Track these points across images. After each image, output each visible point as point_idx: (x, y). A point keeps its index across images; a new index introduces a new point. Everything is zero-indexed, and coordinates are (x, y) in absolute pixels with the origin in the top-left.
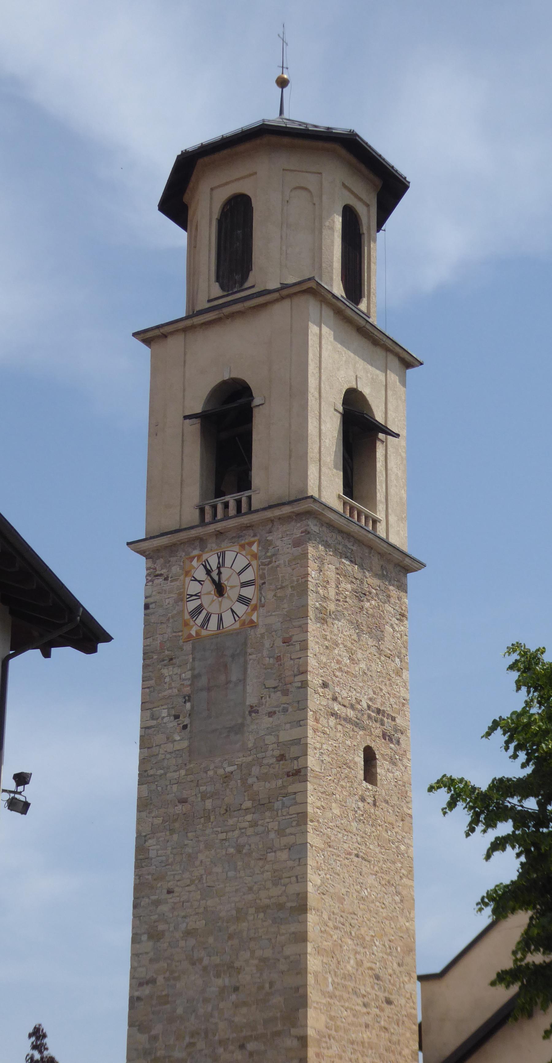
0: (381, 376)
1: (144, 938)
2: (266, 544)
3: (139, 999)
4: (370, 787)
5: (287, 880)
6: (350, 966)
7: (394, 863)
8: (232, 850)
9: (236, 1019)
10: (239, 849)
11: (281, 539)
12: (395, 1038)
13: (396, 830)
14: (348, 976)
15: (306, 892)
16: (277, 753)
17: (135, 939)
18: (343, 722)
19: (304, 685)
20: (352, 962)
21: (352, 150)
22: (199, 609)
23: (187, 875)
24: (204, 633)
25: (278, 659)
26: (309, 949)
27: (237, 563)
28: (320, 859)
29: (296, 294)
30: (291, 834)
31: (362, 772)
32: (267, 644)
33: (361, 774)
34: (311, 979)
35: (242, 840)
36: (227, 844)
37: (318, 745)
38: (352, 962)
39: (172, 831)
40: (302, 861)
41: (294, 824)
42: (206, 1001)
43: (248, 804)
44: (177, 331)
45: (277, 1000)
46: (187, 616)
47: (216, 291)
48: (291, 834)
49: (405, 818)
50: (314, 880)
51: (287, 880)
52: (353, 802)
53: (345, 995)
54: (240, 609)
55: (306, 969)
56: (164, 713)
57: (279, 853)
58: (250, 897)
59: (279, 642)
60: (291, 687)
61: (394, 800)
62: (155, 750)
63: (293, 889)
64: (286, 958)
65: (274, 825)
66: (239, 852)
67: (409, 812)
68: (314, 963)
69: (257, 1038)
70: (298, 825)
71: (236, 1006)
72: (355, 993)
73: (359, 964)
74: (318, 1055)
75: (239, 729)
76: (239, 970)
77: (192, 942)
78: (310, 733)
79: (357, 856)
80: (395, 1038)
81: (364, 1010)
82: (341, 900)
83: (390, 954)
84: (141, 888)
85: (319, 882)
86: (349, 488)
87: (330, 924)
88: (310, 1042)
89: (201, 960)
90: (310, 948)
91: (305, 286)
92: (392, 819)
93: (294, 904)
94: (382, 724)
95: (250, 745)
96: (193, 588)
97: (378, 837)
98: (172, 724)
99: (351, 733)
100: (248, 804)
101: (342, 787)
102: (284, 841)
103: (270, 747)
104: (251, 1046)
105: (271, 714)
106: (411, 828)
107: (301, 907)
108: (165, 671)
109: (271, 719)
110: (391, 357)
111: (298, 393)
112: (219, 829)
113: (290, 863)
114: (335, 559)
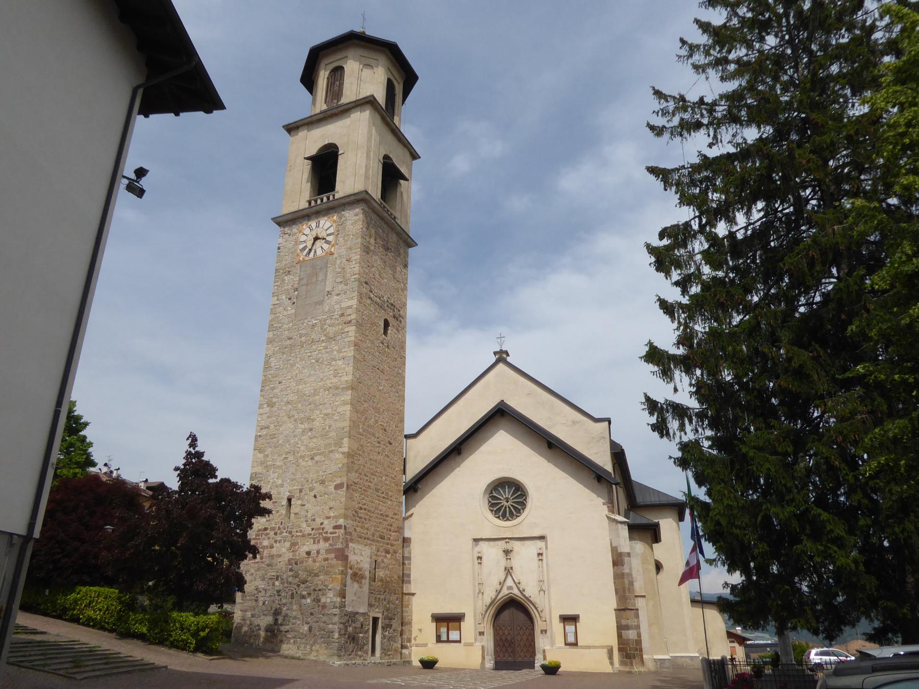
3: (260, 436)
6: (372, 422)
16: (340, 313)
24: (307, 258)
25: (343, 269)
32: (338, 262)
35: (320, 355)
39: (283, 353)
43: (324, 338)
45: (332, 434)
46: (299, 251)
52: (377, 343)
59: (344, 260)
73: (377, 422)
75: (321, 303)
76: (313, 420)
77: (290, 406)
86: (383, 196)
89: (293, 416)
98: (288, 302)
100: (324, 338)
102: (341, 355)
105: (338, 295)
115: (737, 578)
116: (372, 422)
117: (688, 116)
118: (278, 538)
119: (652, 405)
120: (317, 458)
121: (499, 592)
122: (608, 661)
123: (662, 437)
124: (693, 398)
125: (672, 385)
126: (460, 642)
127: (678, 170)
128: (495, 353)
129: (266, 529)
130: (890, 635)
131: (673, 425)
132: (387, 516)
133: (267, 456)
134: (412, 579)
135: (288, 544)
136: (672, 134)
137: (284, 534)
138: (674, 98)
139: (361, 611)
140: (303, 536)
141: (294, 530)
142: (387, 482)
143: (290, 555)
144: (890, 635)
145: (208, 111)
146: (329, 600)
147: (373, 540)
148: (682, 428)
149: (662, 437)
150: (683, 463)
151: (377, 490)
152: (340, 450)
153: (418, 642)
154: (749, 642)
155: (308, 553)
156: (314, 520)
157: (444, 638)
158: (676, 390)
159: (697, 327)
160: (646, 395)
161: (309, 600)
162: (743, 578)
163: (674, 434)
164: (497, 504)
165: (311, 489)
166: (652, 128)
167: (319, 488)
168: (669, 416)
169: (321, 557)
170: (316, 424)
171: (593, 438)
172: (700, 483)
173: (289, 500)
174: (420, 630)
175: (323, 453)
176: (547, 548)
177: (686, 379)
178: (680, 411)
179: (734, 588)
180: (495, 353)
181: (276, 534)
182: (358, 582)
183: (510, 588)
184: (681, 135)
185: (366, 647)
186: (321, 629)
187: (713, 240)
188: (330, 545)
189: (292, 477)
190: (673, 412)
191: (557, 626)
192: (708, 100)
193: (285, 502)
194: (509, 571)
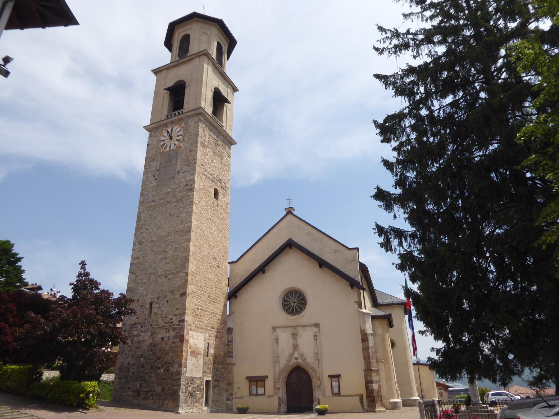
0: (227, 89)
1: (137, 244)
2: (186, 124)
3: (133, 264)
11: (191, 122)
12: (220, 279)
17: (134, 245)
19: (195, 163)
21: (220, 24)
22: (164, 144)
23: (153, 224)
25: (188, 156)
27: (177, 130)
28: (197, 217)
29: (201, 55)
33: (213, 196)
34: (191, 254)
39: (149, 210)
40: (191, 216)
42: (155, 263)
43: (175, 200)
44: (165, 69)
45: (179, 261)
47: (178, 58)
50: (194, 223)
53: (203, 262)
54: (177, 143)
56: (150, 175)
58: (173, 229)
60: (191, 164)
62: (146, 187)
65: (182, 206)
66: (170, 215)
68: (192, 249)
71: (165, 264)
73: (209, 253)
74: (192, 279)
75: (173, 178)
76: (167, 252)
77: (152, 244)
78: (196, 177)
82: (204, 231)
84: (138, 229)
90: (191, 244)
91: (204, 53)
96: (163, 138)
97: (218, 216)
98: (152, 178)
100: (175, 200)
102: (185, 210)
104: (169, 277)
105: (184, 173)
107: (189, 230)
108: (152, 163)
110: (229, 85)
111: (199, 82)
114: (209, 131)
115: (440, 344)
117: (402, 42)
118: (143, 329)
119: (380, 230)
120: (169, 277)
121: (289, 361)
122: (359, 405)
123: (387, 251)
124: (407, 222)
125: (392, 214)
126: (264, 394)
127: (394, 75)
129: (136, 324)
130: (544, 381)
131: (395, 242)
132: (216, 314)
133: (137, 276)
135: (149, 334)
136: (389, 52)
137: (147, 327)
138: (391, 31)
139: (198, 376)
140: (160, 327)
141: (154, 324)
142: (217, 292)
143: (151, 341)
144: (544, 381)
145: (66, 25)
146: (175, 370)
148: (400, 244)
149: (387, 251)
150: (402, 267)
151: (209, 297)
153: (238, 395)
154: (450, 389)
155: (162, 339)
156: (166, 317)
157: (254, 392)
158: (395, 217)
159: (408, 174)
160: (376, 223)
161: (162, 370)
162: (445, 344)
163: (395, 249)
164: (288, 305)
165: (165, 297)
166: (377, 49)
167: (170, 296)
168: (392, 237)
169: (170, 341)
170: (169, 255)
171: (348, 261)
172: (414, 281)
173: (151, 304)
174: (239, 388)
175: (173, 273)
176: (319, 332)
177: (402, 210)
178: (399, 234)
179: (438, 351)
180: (285, 209)
181: (142, 327)
182: (195, 357)
183: (296, 358)
184: (395, 54)
185: (201, 400)
187: (420, 119)
188: (177, 333)
190: (394, 234)
191: (327, 382)
192: (412, 31)
193: (148, 306)
194: (295, 347)
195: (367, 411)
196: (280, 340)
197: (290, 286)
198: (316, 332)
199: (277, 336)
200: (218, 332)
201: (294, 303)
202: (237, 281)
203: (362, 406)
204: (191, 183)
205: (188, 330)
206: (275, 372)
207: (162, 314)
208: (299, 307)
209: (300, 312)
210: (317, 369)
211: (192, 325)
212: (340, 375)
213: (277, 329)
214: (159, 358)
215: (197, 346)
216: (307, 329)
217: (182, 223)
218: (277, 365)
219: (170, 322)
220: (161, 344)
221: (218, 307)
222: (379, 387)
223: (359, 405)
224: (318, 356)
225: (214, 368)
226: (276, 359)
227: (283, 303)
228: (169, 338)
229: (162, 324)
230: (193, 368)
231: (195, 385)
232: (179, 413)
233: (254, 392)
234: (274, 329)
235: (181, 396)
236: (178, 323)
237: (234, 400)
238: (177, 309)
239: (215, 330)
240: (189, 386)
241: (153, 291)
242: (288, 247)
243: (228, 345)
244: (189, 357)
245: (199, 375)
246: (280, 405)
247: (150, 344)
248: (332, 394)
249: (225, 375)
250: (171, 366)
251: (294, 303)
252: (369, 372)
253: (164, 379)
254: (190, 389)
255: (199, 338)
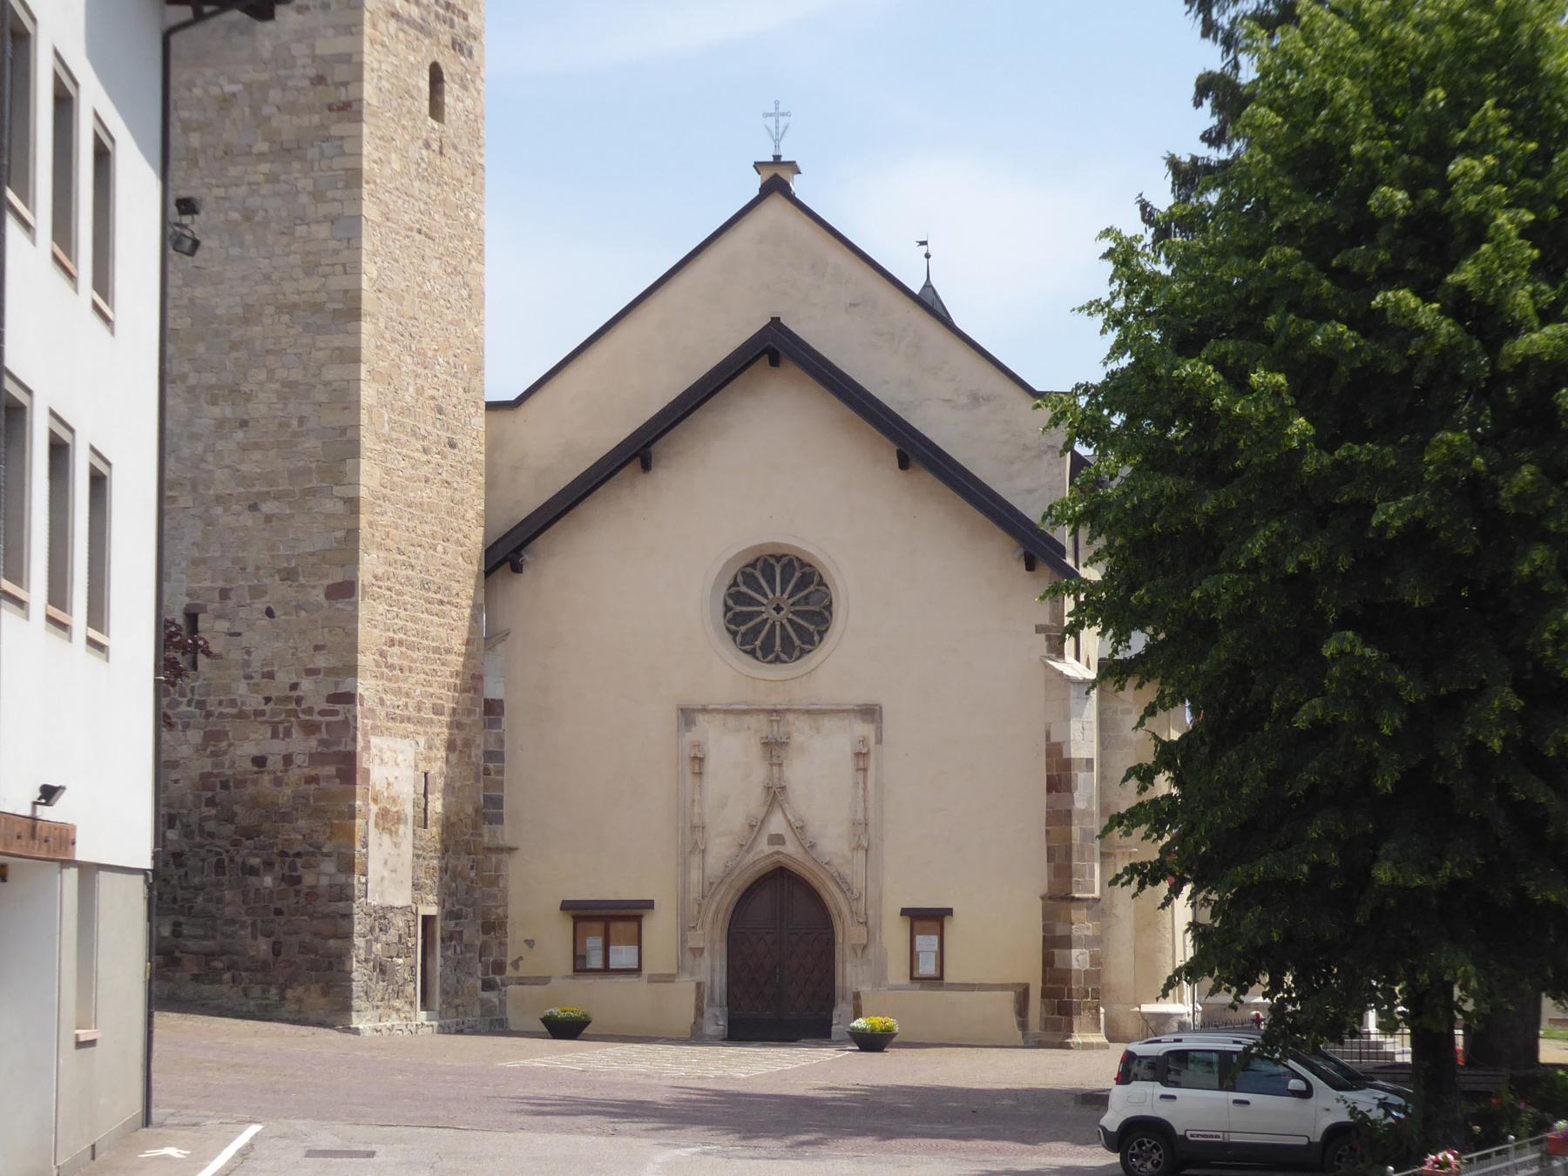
4: (436, 125)
5: (328, 270)
6: (408, 396)
7: (462, 240)
8: (235, 215)
9: (244, 468)
10: (248, 216)
12: (458, 496)
13: (466, 189)
14: (407, 411)
15: (359, 290)
16: (311, 72)
18: (405, 27)
20: (411, 389)
26: (363, 374)
28: (376, 240)
30: (335, 200)
31: (427, 103)
34: (364, 418)
35: (254, 202)
36: (227, 205)
37: (376, 65)
38: (411, 389)
41: (340, 185)
42: (194, 437)
43: (263, 147)
45: (311, 444)
48: (335, 200)
49: (475, 170)
51: (328, 270)
52: (416, 151)
53: (403, 438)
55: (359, 402)
57: (314, 228)
58: (266, 289)
61: (463, 147)
63: (339, 282)
64: (327, 384)
65: (306, 184)
67: (480, 161)
68: (368, 393)
69: (277, 497)
70: (347, 187)
71: (244, 448)
72: (414, 434)
73: (420, 391)
74: (371, 524)
76: (248, 397)
79: (419, 232)
80: (458, 496)
81: (425, 458)
83: (454, 376)
85: (375, 275)
87: (387, 336)
88: (363, 509)
92: (460, 173)
93: (339, 306)
94: (452, 26)
95: (266, 54)
99: (415, 43)
100: (263, 147)
101: (404, 127)
102: (323, 209)
103: (300, 62)
104: (268, 507)
106: (482, 187)
107: (352, 311)
109: (301, 17)
112: (214, 181)
113: (333, 244)
116: (408, 396)
121: (745, 847)
126: (637, 971)
128: (758, 166)
134: (505, 810)
135: (195, 736)
139: (399, 903)
140: (242, 715)
141: (212, 700)
142: (448, 558)
143: (207, 765)
146: (324, 881)
147: (420, 722)
151: (424, 585)
152: (337, 490)
153: (525, 970)
155: (260, 761)
156: (270, 676)
157: (595, 961)
161: (268, 881)
165: (257, 592)
167: (278, 591)
170: (257, 409)
171: (1025, 448)
174: (530, 943)
176: (879, 741)
180: (758, 166)
182: (391, 832)
183: (777, 839)
185: (409, 989)
186: (305, 949)
188: (322, 742)
189: (196, 553)
191: (894, 934)
194: (775, 795)
195: (1040, 1044)
196: (711, 765)
197: (765, 540)
198: (864, 741)
199: (698, 745)
200: (455, 725)
201: (778, 609)
202: (529, 498)
203: (1023, 1025)
204: (341, 72)
205: (365, 735)
206: (685, 889)
207: (247, 664)
208: (799, 629)
209: (803, 652)
210: (858, 883)
211: (379, 709)
212: (949, 912)
213: (700, 718)
214: (250, 833)
215: (394, 792)
216: (828, 724)
217: (310, 269)
218: (696, 860)
219: (287, 699)
220: (255, 782)
221: (451, 628)
222: (1096, 960)
223: (1012, 1020)
224: (864, 835)
225: (444, 870)
226: (692, 836)
227: (728, 609)
228: (288, 760)
229: (255, 702)
230: (386, 874)
231: (392, 936)
232: (356, 1031)
233: (595, 961)
234: (687, 716)
235: (355, 975)
236: (325, 706)
237: (511, 988)
238: (317, 648)
239: (445, 719)
240: (377, 940)
241: (195, 562)
242: (765, 359)
243: (487, 772)
244: (373, 834)
245: (402, 898)
246: (699, 1011)
247: (205, 777)
248: (912, 978)
249: (477, 895)
250: (308, 866)
251: (778, 609)
252: (1063, 904)
253: (278, 912)
254: (377, 947)
255: (400, 758)
